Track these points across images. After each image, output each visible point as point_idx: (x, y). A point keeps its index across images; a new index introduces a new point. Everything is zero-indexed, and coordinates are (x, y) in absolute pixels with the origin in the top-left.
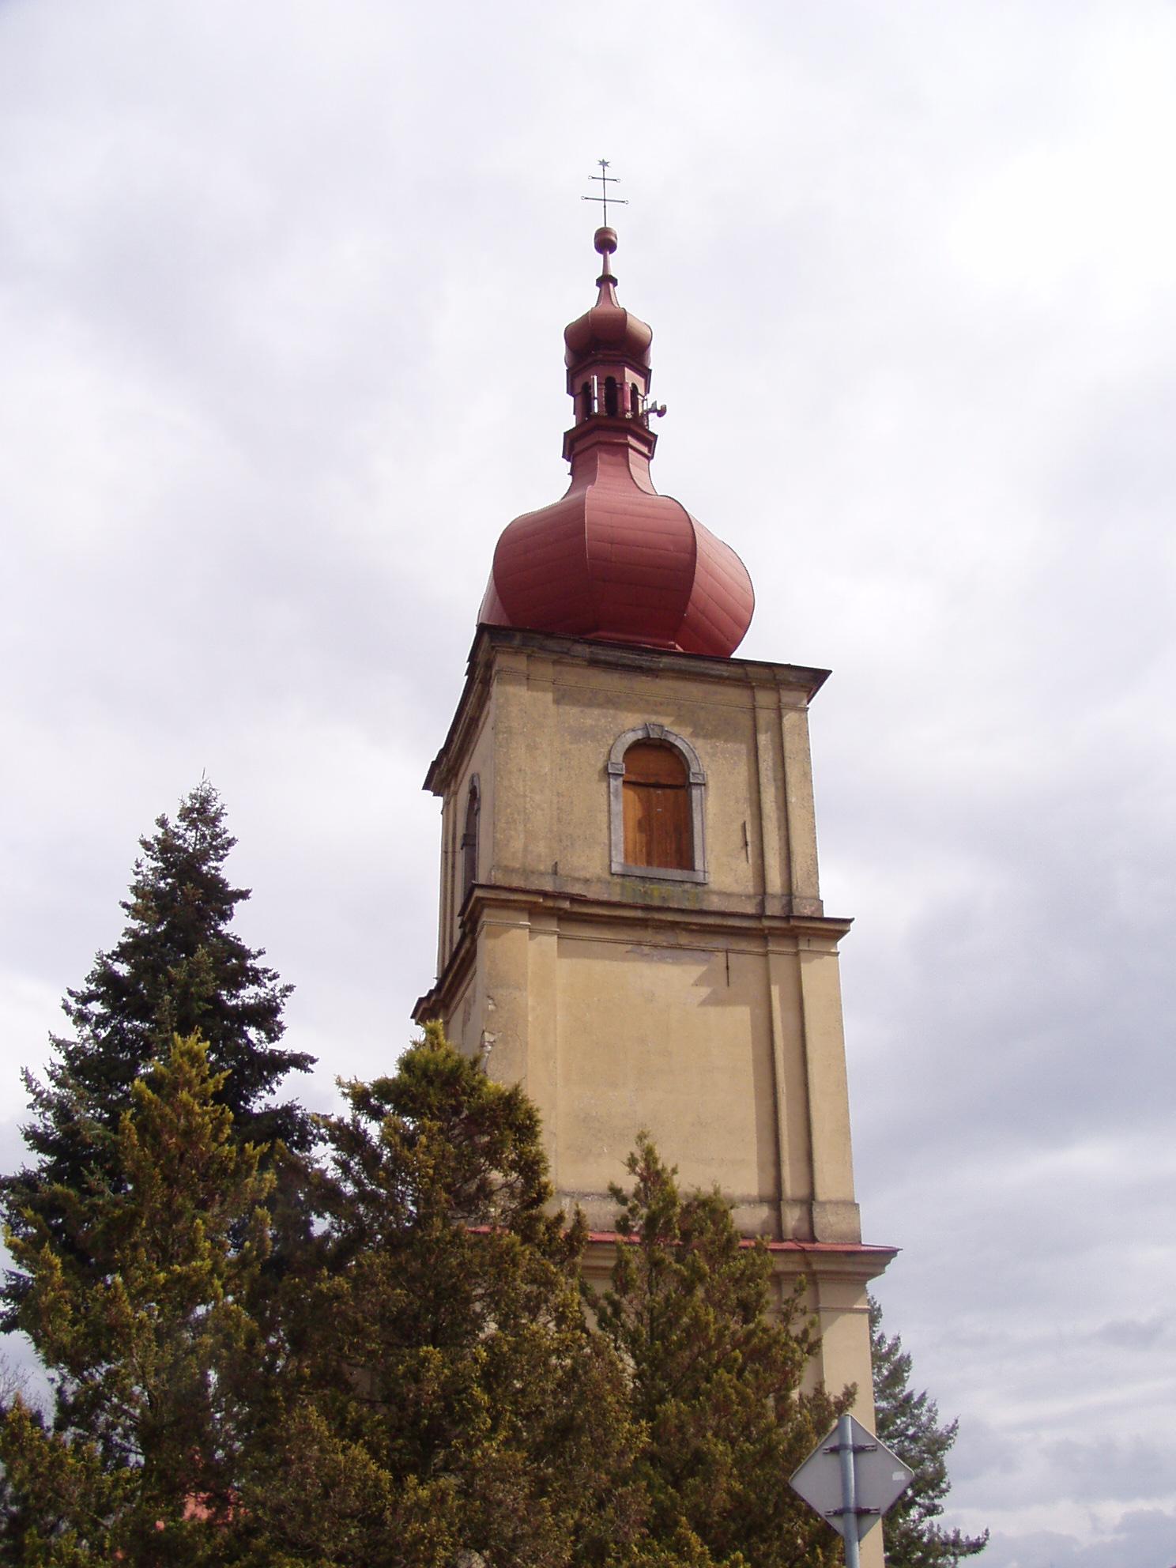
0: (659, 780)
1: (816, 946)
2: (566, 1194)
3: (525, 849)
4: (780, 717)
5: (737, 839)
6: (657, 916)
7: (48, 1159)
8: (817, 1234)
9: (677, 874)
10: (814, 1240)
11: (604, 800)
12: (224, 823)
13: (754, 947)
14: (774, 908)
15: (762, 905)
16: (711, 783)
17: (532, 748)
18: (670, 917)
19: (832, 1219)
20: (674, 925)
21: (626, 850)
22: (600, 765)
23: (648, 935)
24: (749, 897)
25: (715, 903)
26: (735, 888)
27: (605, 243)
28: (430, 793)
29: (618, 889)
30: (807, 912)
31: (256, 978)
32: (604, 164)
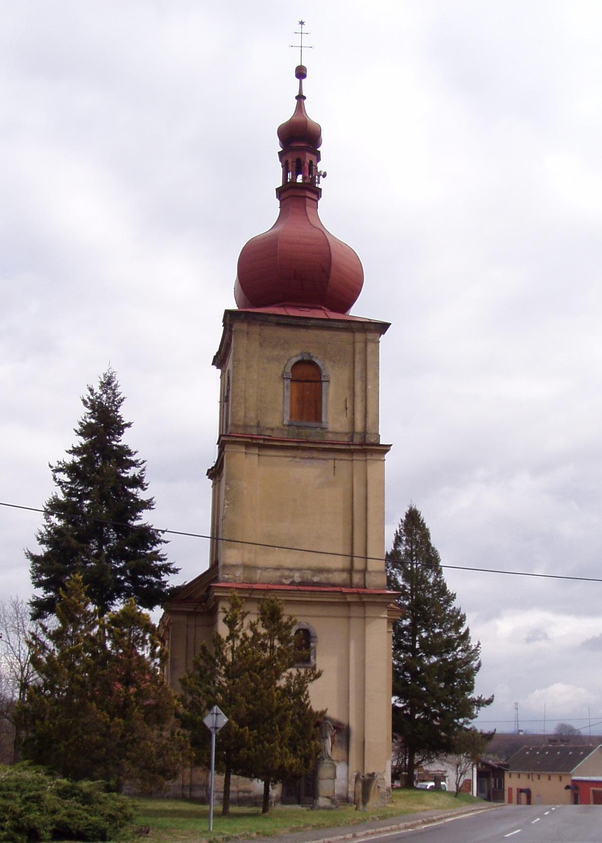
0: (307, 379)
1: (375, 457)
2: (259, 568)
3: (245, 416)
4: (366, 347)
5: (342, 407)
8: (367, 585)
9: (314, 424)
10: (365, 588)
11: (281, 391)
14: (357, 439)
15: (352, 438)
16: (332, 380)
17: (248, 367)
19: (374, 579)
20: (311, 449)
22: (280, 374)
23: (299, 453)
25: (330, 437)
26: (340, 430)
27: (301, 73)
28: (214, 367)
29: (286, 433)
30: (372, 440)
31: (134, 464)
32: (302, 23)
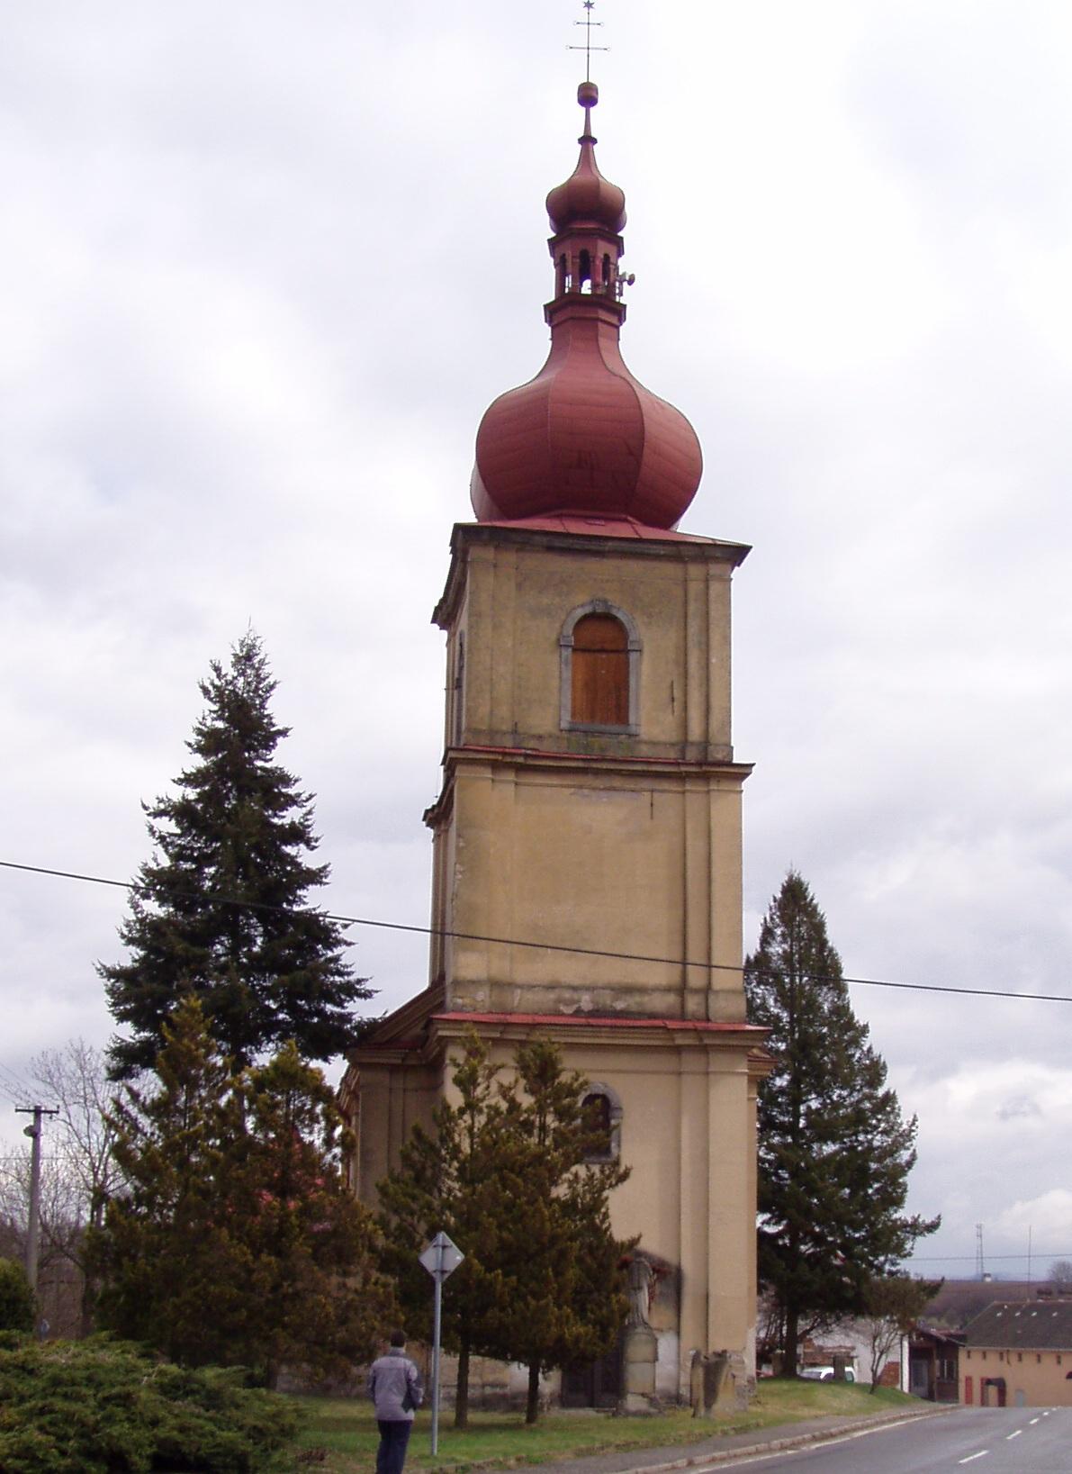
0: (601, 644)
1: (725, 786)
4: (707, 588)
5: (665, 695)
6: (595, 765)
7: (142, 953)
10: (708, 1020)
12: (266, 670)
13: (674, 786)
14: (692, 755)
15: (683, 752)
16: (646, 650)
18: (605, 766)
20: (609, 772)
21: (574, 707)
22: (554, 637)
23: (589, 780)
24: (672, 745)
25: (644, 751)
26: (663, 738)
27: (588, 96)
28: (436, 626)
31: (292, 801)
